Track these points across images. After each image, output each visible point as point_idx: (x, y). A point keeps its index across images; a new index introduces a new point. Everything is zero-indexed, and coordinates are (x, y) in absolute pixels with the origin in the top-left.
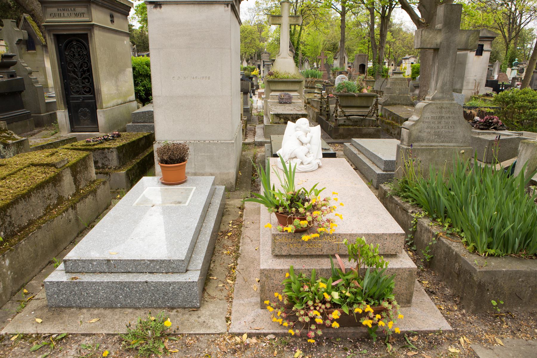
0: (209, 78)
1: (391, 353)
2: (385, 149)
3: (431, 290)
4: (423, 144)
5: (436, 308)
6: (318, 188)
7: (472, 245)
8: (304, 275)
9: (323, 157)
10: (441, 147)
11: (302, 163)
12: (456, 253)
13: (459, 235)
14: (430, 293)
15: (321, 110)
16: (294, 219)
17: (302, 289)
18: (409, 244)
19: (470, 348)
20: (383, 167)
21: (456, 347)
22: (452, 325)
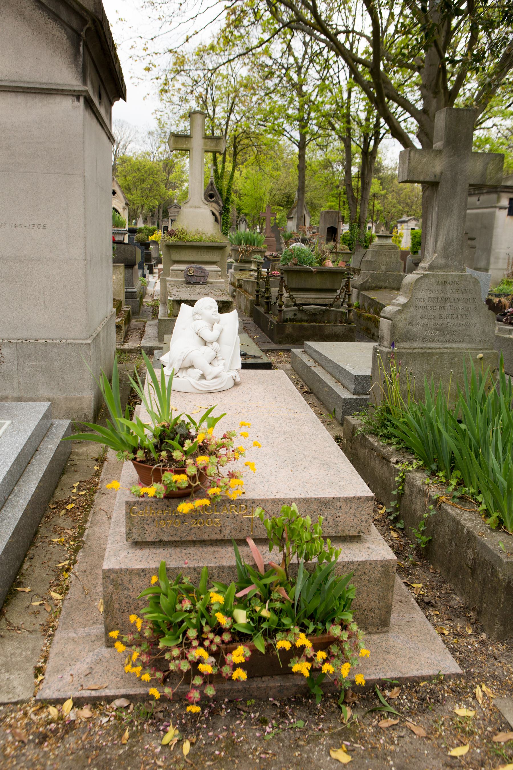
0: (45, 227)
1: (348, 725)
2: (355, 357)
3: (426, 600)
4: (415, 345)
5: (435, 632)
6: (214, 414)
7: (495, 515)
8: (186, 580)
9: (243, 368)
10: (446, 351)
11: (203, 377)
12: (468, 531)
13: (475, 500)
14: (425, 604)
15: (257, 296)
16: (163, 471)
17: (178, 607)
18: (392, 518)
19: (494, 705)
20: (352, 387)
21: (468, 705)
22: (461, 663)
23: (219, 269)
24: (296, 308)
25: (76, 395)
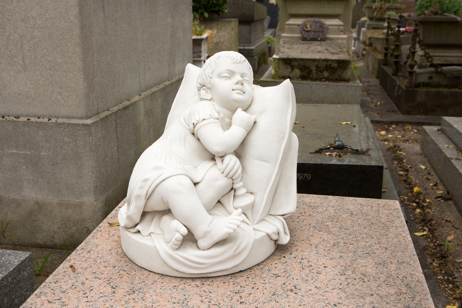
11: (190, 239)
15: (386, 55)
23: (341, 23)
24: (432, 69)
25: (74, 200)
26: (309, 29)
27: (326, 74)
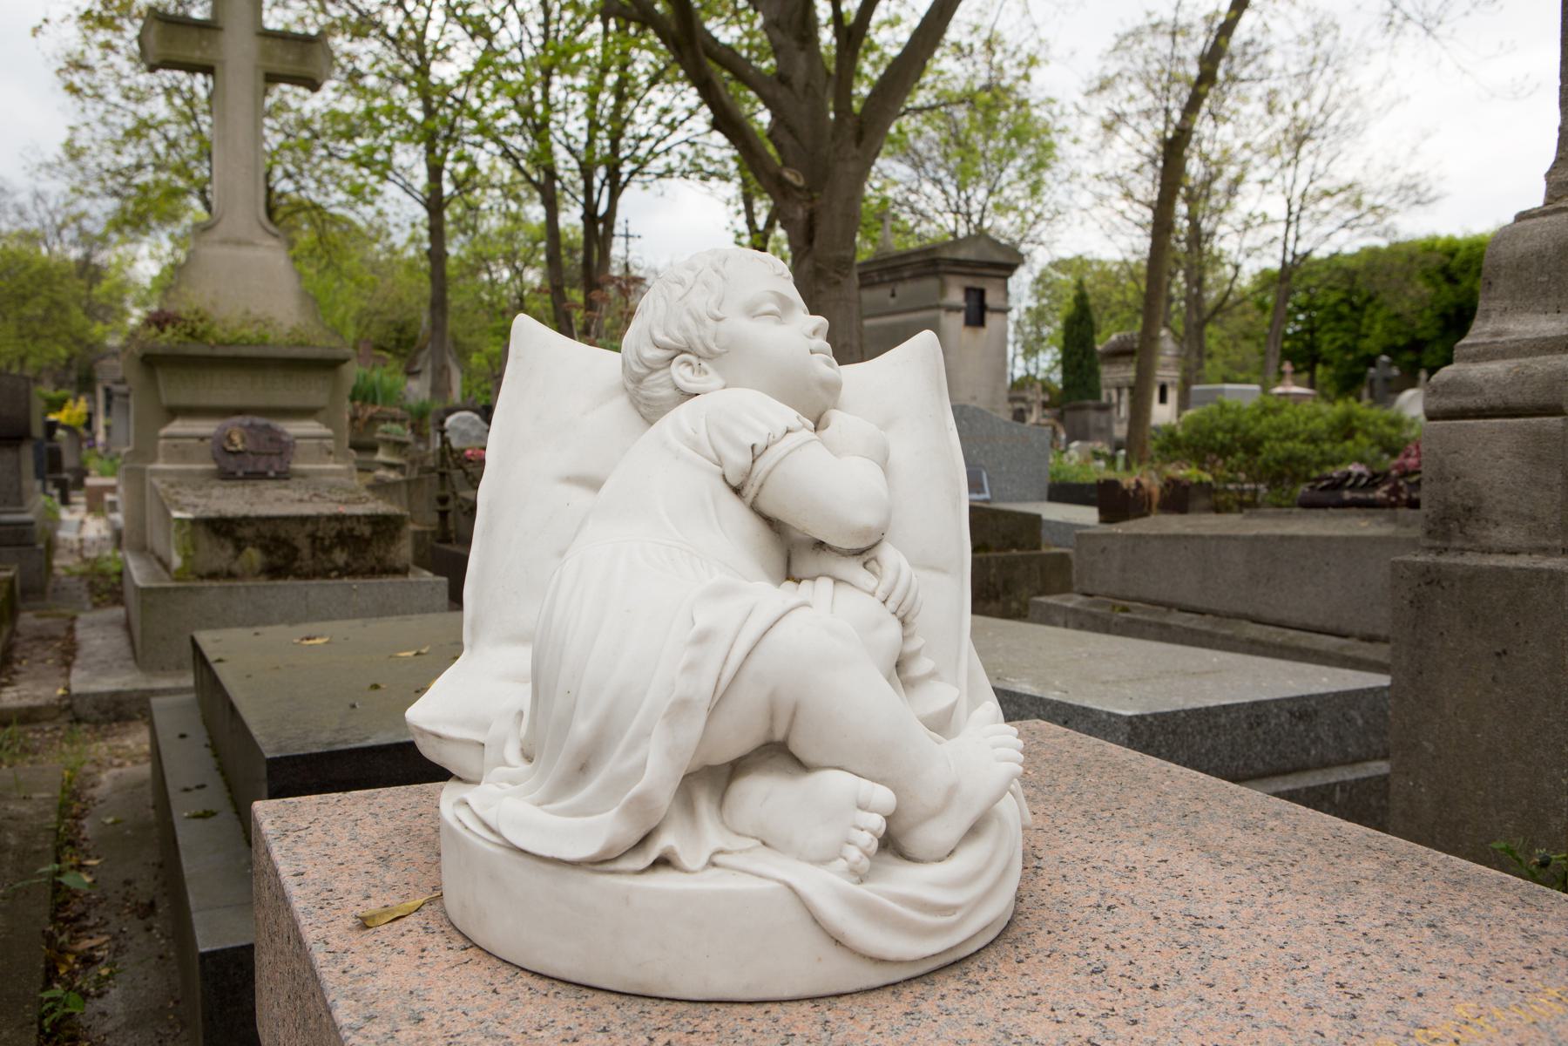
15: (443, 515)
23: (329, 432)
26: (240, 447)
27: (340, 557)
